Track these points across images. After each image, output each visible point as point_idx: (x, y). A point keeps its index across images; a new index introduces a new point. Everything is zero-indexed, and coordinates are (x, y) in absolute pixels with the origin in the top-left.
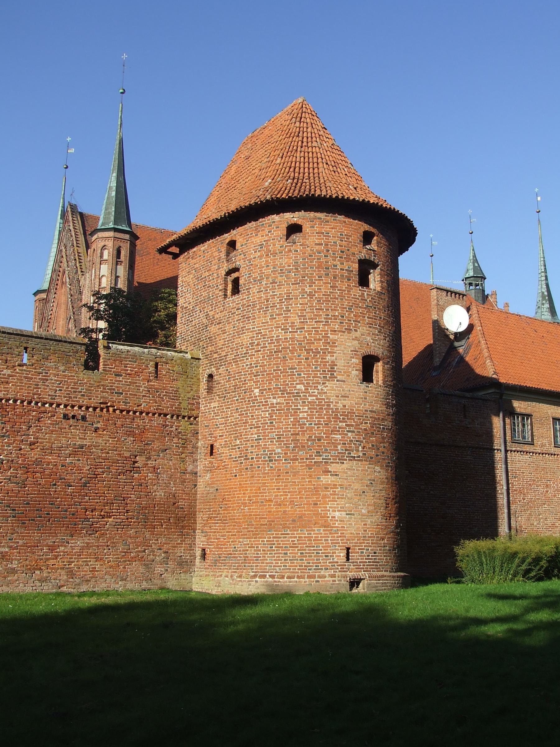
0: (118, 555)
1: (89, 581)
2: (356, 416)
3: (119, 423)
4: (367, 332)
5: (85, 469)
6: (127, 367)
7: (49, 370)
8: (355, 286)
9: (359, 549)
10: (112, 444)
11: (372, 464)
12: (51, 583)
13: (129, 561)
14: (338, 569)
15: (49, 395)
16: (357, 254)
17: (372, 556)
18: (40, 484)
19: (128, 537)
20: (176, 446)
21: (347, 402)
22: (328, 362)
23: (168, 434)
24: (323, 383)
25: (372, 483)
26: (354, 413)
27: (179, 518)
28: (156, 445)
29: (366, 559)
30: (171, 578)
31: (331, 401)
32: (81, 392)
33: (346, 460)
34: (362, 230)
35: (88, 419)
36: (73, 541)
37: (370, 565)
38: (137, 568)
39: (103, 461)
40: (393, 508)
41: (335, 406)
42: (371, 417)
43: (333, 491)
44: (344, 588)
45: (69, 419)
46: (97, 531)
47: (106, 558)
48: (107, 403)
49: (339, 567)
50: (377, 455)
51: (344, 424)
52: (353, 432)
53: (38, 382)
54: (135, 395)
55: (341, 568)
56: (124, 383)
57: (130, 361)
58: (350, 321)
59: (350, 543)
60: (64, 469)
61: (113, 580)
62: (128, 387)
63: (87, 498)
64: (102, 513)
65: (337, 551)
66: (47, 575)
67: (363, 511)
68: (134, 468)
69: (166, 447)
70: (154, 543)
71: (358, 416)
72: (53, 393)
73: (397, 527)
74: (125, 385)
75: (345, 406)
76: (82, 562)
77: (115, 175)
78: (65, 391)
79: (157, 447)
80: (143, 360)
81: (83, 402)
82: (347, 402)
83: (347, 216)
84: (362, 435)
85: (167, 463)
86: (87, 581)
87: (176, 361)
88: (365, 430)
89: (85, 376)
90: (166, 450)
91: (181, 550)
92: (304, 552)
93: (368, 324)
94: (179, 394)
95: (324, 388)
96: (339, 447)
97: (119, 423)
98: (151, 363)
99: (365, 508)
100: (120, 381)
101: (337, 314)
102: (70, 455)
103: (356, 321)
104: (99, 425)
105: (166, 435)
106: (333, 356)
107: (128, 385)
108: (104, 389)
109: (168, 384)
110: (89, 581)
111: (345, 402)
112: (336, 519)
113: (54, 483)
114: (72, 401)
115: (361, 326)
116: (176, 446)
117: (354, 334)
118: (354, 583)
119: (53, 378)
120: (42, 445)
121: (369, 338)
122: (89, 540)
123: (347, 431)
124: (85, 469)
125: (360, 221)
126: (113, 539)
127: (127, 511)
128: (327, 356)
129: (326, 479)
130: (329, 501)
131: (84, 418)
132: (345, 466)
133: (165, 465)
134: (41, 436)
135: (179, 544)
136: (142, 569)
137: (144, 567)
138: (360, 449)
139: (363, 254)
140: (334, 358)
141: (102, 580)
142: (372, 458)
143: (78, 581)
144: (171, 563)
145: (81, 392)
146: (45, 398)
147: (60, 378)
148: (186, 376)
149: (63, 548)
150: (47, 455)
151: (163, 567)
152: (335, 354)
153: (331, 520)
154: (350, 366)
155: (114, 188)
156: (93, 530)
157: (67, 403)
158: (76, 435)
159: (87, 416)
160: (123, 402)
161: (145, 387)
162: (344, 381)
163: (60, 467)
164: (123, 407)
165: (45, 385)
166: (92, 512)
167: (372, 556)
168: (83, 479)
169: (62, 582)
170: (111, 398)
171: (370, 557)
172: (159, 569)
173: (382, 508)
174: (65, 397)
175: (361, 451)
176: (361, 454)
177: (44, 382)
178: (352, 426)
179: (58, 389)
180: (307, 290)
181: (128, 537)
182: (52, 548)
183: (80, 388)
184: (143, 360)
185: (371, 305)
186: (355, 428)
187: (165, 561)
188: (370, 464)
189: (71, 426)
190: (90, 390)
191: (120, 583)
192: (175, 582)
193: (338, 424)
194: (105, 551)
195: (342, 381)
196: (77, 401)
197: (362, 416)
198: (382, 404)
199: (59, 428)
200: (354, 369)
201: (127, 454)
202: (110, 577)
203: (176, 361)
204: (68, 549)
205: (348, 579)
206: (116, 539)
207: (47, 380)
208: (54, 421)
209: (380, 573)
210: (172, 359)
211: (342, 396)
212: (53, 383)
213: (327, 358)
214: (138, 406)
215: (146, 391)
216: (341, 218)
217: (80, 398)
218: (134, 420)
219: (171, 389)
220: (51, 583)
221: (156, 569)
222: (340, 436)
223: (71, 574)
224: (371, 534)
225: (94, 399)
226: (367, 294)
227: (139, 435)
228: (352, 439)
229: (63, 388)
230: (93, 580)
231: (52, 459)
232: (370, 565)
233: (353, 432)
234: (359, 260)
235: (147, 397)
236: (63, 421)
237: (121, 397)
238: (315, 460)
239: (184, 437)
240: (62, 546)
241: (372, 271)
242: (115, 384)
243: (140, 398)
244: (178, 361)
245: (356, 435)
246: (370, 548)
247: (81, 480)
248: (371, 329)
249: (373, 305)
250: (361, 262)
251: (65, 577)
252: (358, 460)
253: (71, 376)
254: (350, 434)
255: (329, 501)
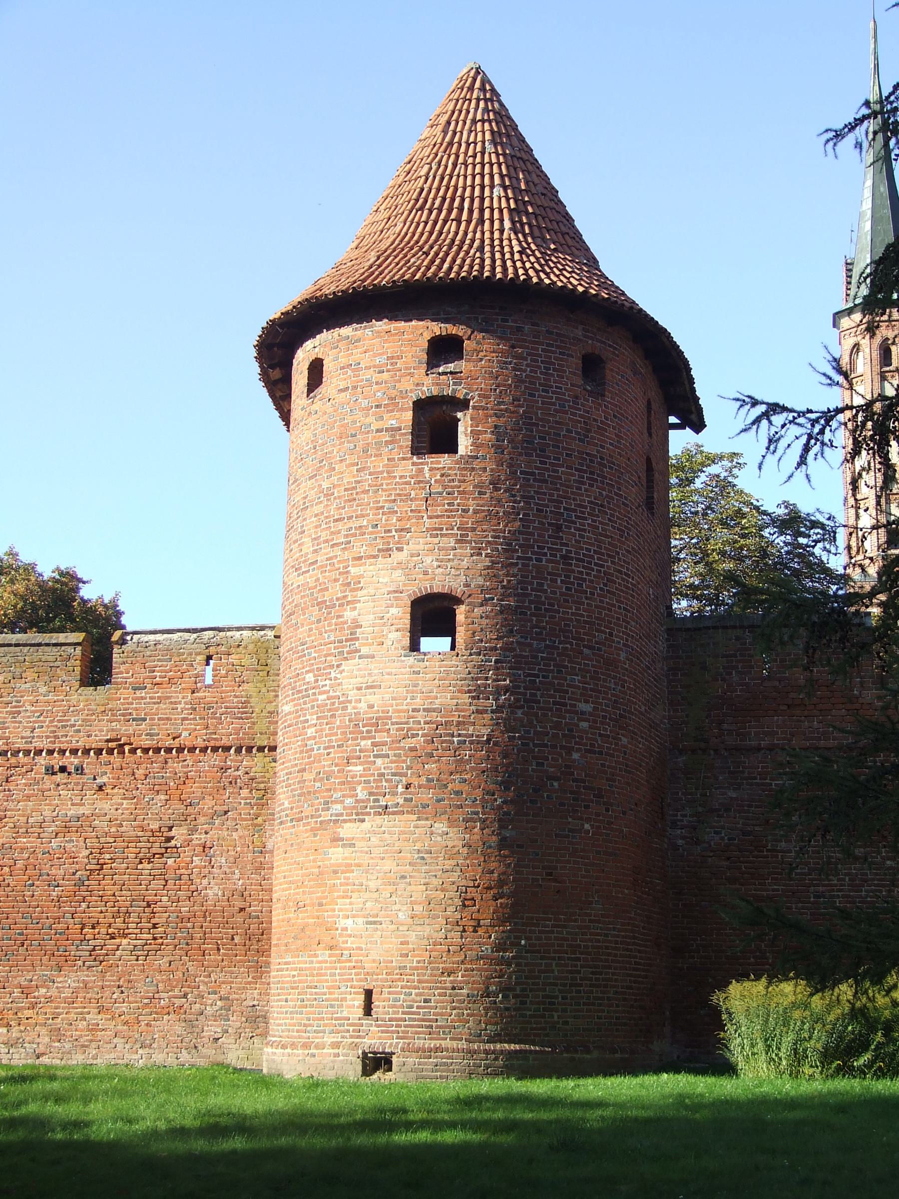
0: (136, 1002)
1: (87, 1046)
2: (393, 724)
3: (140, 773)
4: (426, 547)
5: (81, 855)
6: (154, 671)
7: (22, 697)
8: (404, 459)
9: (389, 993)
10: (128, 809)
11: (427, 819)
12: (25, 1048)
13: (156, 1013)
14: (348, 1031)
15: (22, 738)
16: (411, 391)
17: (418, 1007)
18: (9, 885)
19: (154, 970)
20: (246, 804)
21: (375, 698)
22: (346, 623)
23: (231, 783)
24: (338, 666)
25: (423, 858)
26: (390, 718)
27: (247, 937)
28: (208, 804)
29: (403, 1013)
30: (234, 1046)
31: (349, 698)
32: (74, 726)
33: (369, 814)
34: (428, 336)
35: (86, 771)
36: (61, 979)
37: (411, 1026)
38: (171, 1025)
39: (112, 840)
40: (487, 911)
41: (354, 708)
42: (426, 723)
43: (345, 878)
44: (353, 1070)
45: (54, 774)
46: (101, 962)
47: (117, 1008)
48: (120, 740)
49: (351, 1029)
50: (439, 801)
51: (369, 742)
52: (387, 756)
53: (5, 718)
54: (168, 719)
55: (354, 1031)
56: (148, 700)
57: (159, 660)
58: (390, 531)
59: (372, 980)
60: (46, 858)
61: (127, 1046)
62: (156, 706)
63: (84, 905)
64: (110, 931)
65: (348, 997)
66: (19, 1035)
67: (400, 914)
68: (167, 848)
69: (226, 808)
70: (203, 981)
71: (397, 723)
72: (28, 734)
73: (500, 947)
74: (149, 703)
75: (371, 706)
76: (76, 1013)
77: (869, 183)
78: (48, 727)
79: (209, 809)
80: (183, 654)
81: (78, 741)
82: (375, 698)
83: (393, 318)
84: (404, 761)
85: (230, 836)
86: (83, 1046)
87: (246, 647)
88: (413, 749)
89: (81, 698)
90: (226, 813)
91: (252, 994)
92: (422, 1004)
93: (428, 530)
94: (251, 707)
95: (338, 676)
96: (359, 788)
97: (140, 773)
98: (199, 658)
99: (404, 908)
100: (142, 698)
101: (365, 523)
102: (57, 834)
103: (402, 530)
104: (105, 779)
105: (227, 784)
106: (355, 609)
107: (155, 703)
108: (113, 715)
109: (230, 691)
110: (87, 1046)
111: (372, 699)
112: (349, 932)
113: (31, 882)
114: (60, 742)
115: (412, 537)
116: (246, 804)
117: (397, 557)
118: (376, 1062)
119: (29, 708)
120: (12, 820)
121: (428, 560)
122: (87, 976)
123: (375, 756)
124: (81, 855)
125: (422, 320)
126: (130, 974)
127: (155, 926)
128: (345, 610)
129: (337, 854)
130: (338, 897)
131: (80, 770)
132: (366, 826)
133: (224, 839)
134: (11, 805)
135: (249, 983)
136: (179, 1028)
137: (183, 1024)
138: (400, 789)
139: (429, 385)
140: (356, 612)
141: (109, 1046)
142: (425, 806)
143: (68, 1046)
144: (235, 1018)
145: (74, 726)
146: (16, 743)
147: (40, 706)
148: (265, 673)
149: (45, 990)
150: (20, 837)
151: (218, 1026)
152: (358, 605)
153: (341, 935)
154: (384, 625)
155: (869, 213)
156: (96, 957)
157: (51, 746)
158: (68, 801)
159: (85, 766)
160: (147, 735)
161: (186, 703)
162: (373, 657)
163: (40, 856)
164: (147, 743)
165: (16, 722)
166: (93, 928)
167: (418, 1007)
168: (79, 873)
169: (42, 1049)
170: (125, 730)
171: (414, 1010)
172: (212, 1029)
173: (453, 909)
174: (47, 737)
175: (402, 794)
176: (401, 801)
177: (15, 718)
178: (384, 744)
179: (37, 725)
180: (325, 485)
181: (154, 970)
182: (26, 992)
183: (73, 719)
184: (183, 654)
185: (440, 490)
186: (389, 749)
187: (223, 1015)
188: (419, 819)
189: (58, 785)
190: (89, 721)
191: (140, 1051)
192: (242, 1054)
193: (358, 745)
194: (115, 996)
195: (367, 657)
196: (67, 742)
197: (407, 723)
198: (460, 691)
199: (38, 790)
200: (393, 628)
201: (155, 826)
202: (123, 1040)
203: (246, 647)
204: (53, 992)
205: (360, 1052)
206: (135, 975)
207: (19, 713)
208: (31, 779)
209: (433, 1044)
210: (239, 646)
211: (368, 688)
212: (29, 717)
213: (345, 613)
214: (174, 739)
215: (188, 709)
216: (382, 325)
217: (72, 736)
218: (166, 762)
219: (235, 700)
220: (25, 1048)
221: (206, 1028)
222: (360, 768)
223: (57, 1034)
224: (418, 962)
225: (96, 736)
226: (431, 470)
227: (176, 790)
228: (383, 771)
229: (45, 722)
230: (94, 1045)
231: (28, 842)
232: (411, 1026)
233: (387, 756)
234: (414, 403)
235: (191, 720)
236: (46, 777)
237: (143, 726)
238: (322, 819)
239: (262, 786)
240: (42, 987)
241: (459, 415)
242: (132, 704)
243: (176, 724)
244: (251, 647)
245: (391, 762)
246: (414, 991)
247: (74, 874)
248: (436, 540)
249: (445, 487)
250: (420, 406)
251: (47, 1039)
252: (394, 813)
253: (58, 701)
254: (379, 761)
255: (338, 897)
